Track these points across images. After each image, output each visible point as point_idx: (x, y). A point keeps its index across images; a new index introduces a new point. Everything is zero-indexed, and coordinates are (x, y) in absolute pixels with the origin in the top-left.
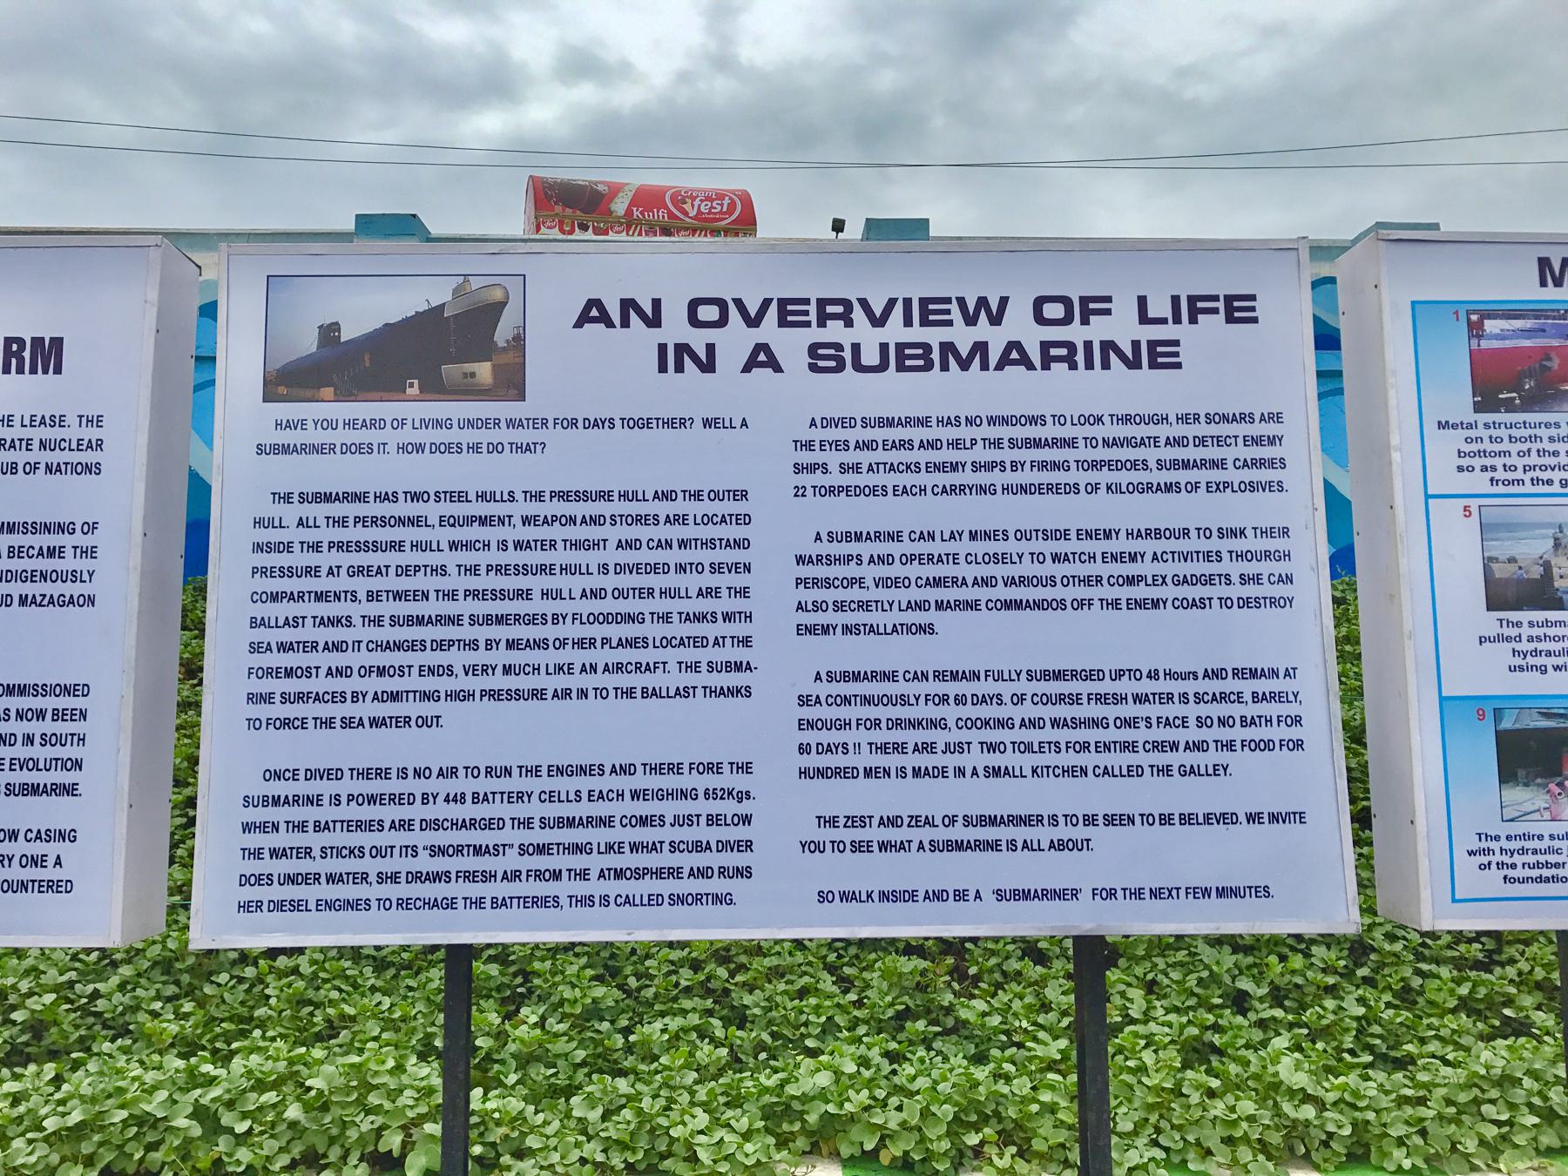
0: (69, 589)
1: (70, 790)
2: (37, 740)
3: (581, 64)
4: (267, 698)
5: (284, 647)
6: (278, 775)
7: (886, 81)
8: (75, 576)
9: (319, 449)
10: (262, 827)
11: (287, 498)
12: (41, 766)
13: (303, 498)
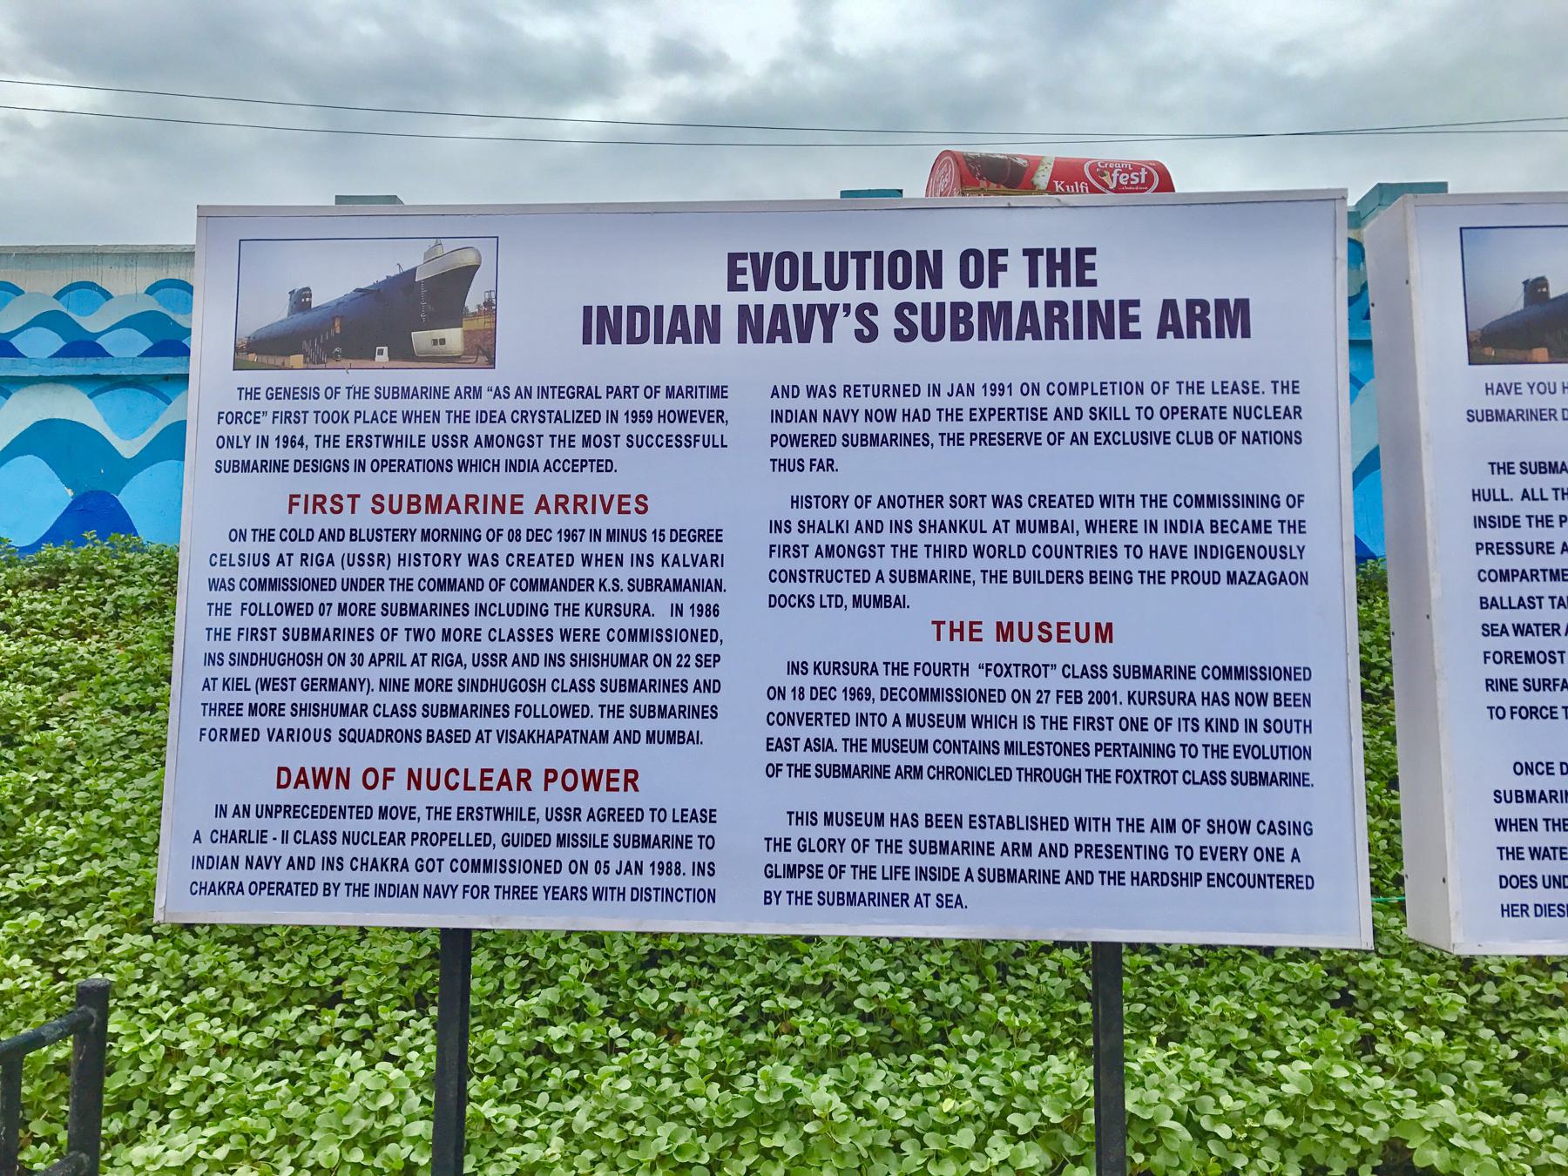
0: (1280, 566)
1: (1300, 780)
2: (1261, 726)
3: (677, 56)
4: (1507, 685)
5: (1520, 630)
6: (1529, 769)
7: (980, 66)
8: (1284, 552)
9: (1536, 415)
10: (1519, 825)
11: (1507, 468)
12: (1268, 753)
13: (1525, 468)
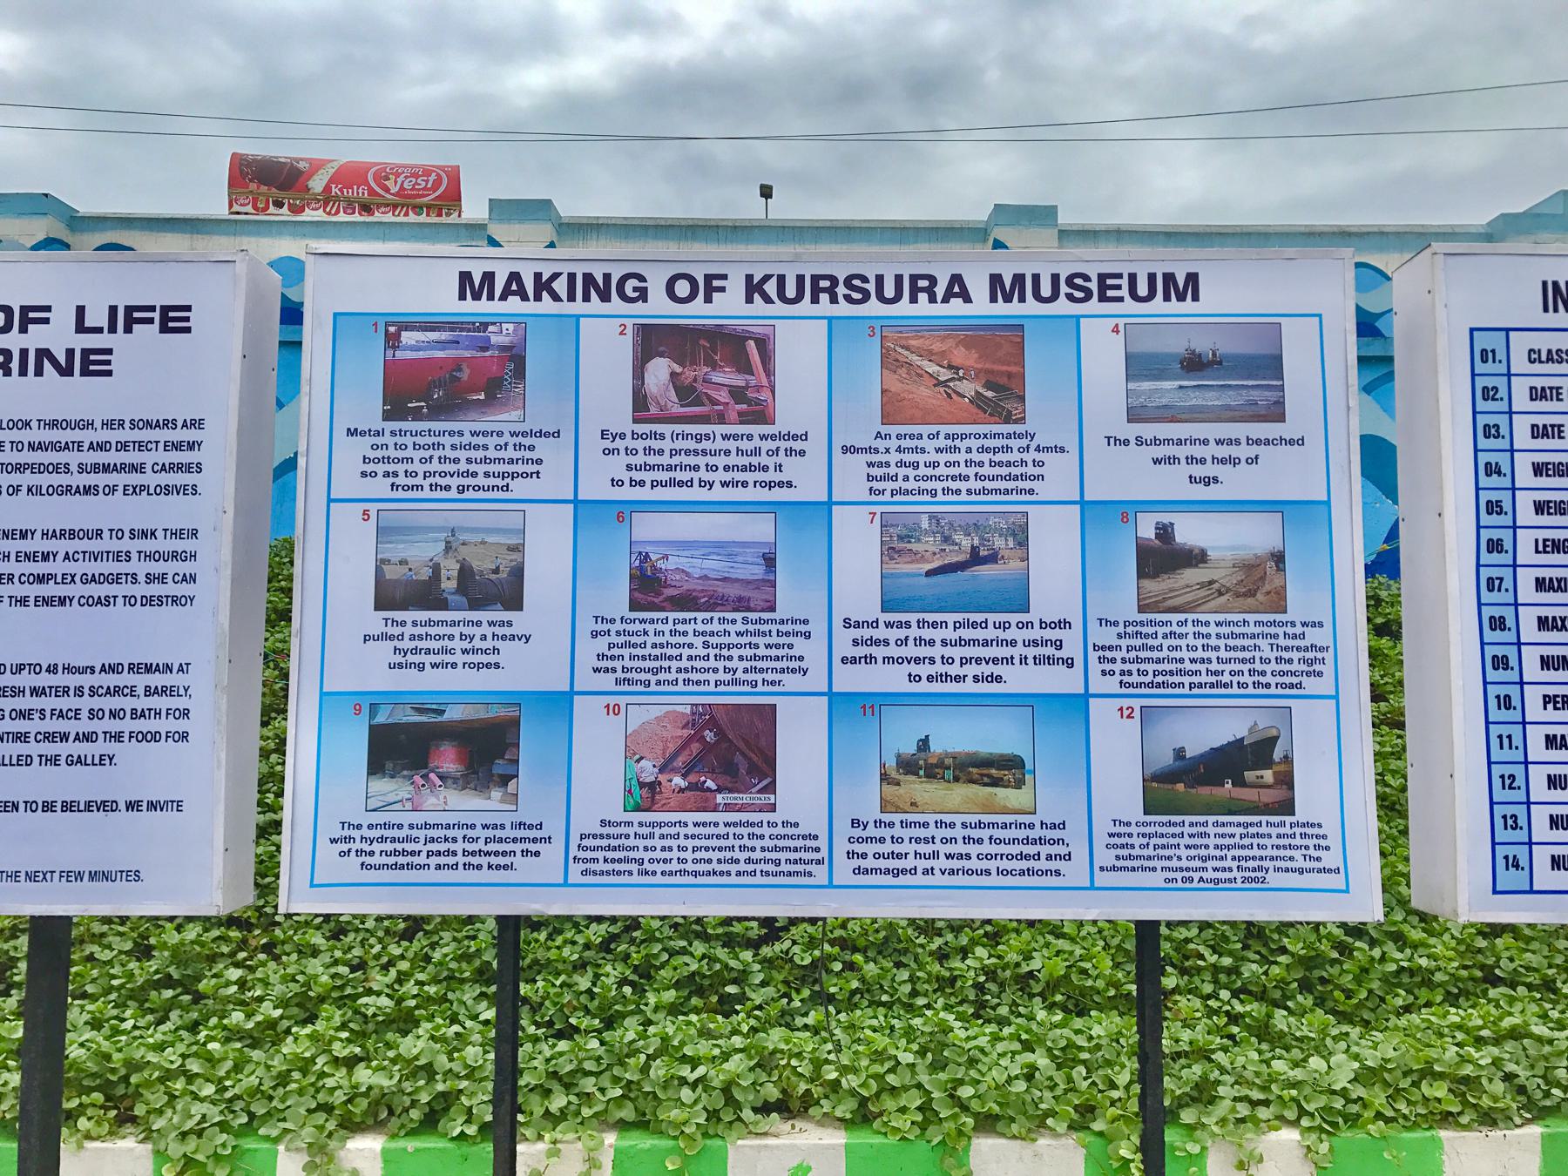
7: (939, 32)
